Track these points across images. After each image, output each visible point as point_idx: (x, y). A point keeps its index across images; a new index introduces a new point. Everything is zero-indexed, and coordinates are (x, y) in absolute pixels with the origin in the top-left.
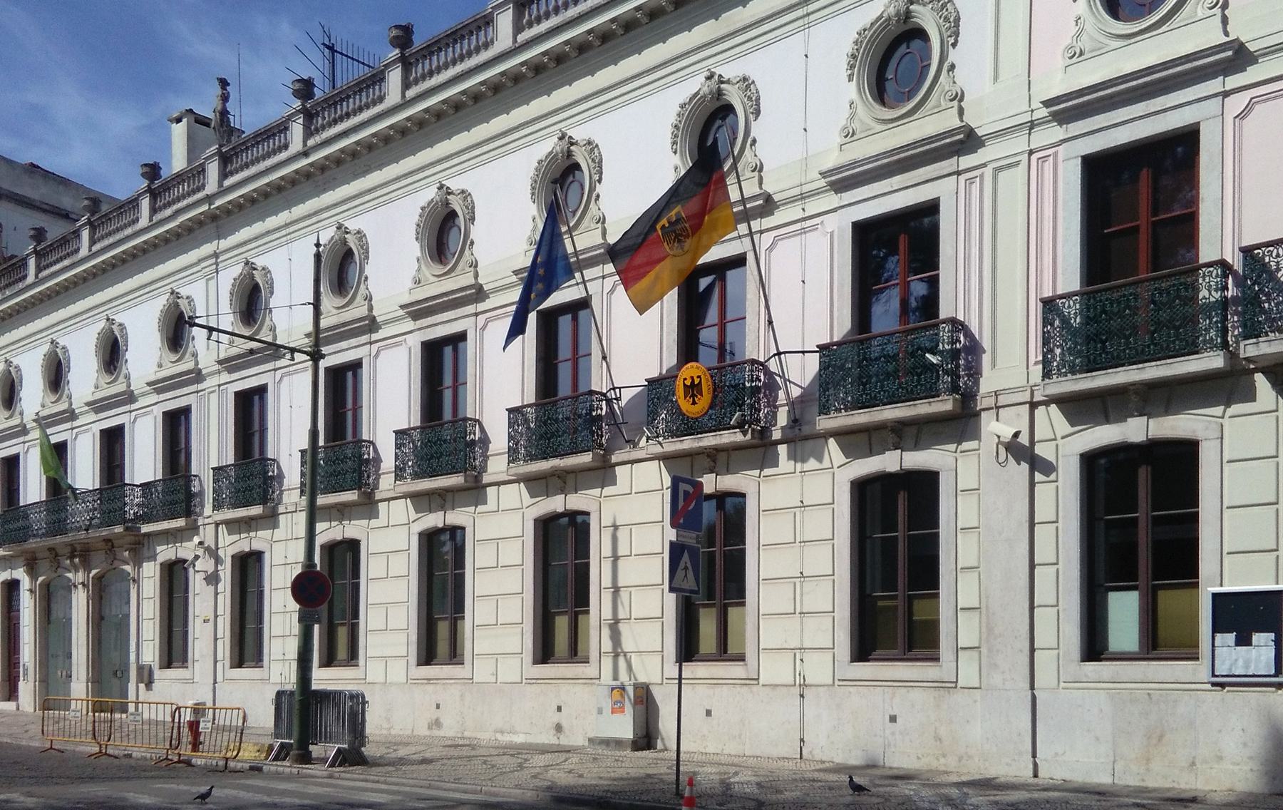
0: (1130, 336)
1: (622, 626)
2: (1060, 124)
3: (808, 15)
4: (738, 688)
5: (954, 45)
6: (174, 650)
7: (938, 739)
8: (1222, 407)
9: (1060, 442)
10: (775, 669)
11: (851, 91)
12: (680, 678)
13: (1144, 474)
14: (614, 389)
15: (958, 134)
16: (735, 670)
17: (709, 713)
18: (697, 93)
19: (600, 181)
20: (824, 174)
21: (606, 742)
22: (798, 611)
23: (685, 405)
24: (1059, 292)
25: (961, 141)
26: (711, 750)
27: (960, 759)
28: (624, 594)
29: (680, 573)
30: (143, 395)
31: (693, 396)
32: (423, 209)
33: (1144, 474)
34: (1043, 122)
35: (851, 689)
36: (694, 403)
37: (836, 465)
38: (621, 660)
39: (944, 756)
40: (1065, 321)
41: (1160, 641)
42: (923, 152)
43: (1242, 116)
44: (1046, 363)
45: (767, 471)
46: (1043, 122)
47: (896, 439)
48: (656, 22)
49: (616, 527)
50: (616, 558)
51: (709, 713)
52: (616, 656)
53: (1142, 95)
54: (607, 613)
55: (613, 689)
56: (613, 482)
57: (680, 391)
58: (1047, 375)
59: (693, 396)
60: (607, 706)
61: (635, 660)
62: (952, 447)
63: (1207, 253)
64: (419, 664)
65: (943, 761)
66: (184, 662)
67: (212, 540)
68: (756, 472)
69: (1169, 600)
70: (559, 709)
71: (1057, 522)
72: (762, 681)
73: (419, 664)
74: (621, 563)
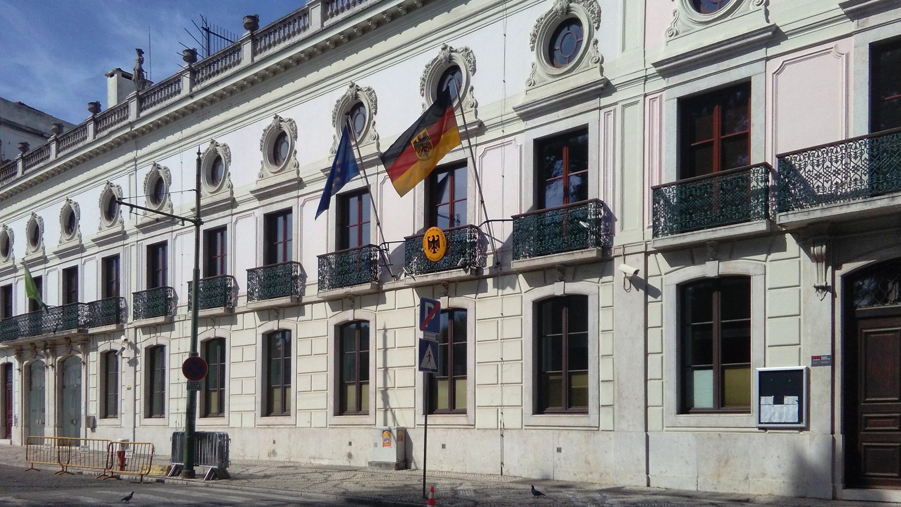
1: (389, 392)
2: (664, 78)
5: (597, 28)
6: (109, 408)
7: (587, 462)
10: (485, 419)
11: (533, 57)
12: (426, 425)
16: (460, 419)
17: (444, 446)
21: (380, 465)
23: (429, 254)
24: (663, 183)
25: (602, 89)
26: (445, 469)
27: (601, 475)
29: (426, 359)
30: (90, 247)
31: (434, 248)
32: (265, 131)
34: (653, 76)
36: (435, 252)
39: (591, 473)
40: (667, 201)
41: (726, 401)
42: (563, 101)
43: (778, 72)
44: (655, 227)
45: (480, 295)
46: (653, 76)
51: (444, 446)
52: (386, 411)
56: (384, 301)
57: (426, 245)
58: (655, 235)
59: (434, 248)
60: (380, 442)
63: (756, 158)
65: (590, 476)
66: (115, 414)
67: (133, 338)
68: (473, 296)
69: (732, 375)
70: (350, 444)
73: (335, 414)
74: (389, 352)
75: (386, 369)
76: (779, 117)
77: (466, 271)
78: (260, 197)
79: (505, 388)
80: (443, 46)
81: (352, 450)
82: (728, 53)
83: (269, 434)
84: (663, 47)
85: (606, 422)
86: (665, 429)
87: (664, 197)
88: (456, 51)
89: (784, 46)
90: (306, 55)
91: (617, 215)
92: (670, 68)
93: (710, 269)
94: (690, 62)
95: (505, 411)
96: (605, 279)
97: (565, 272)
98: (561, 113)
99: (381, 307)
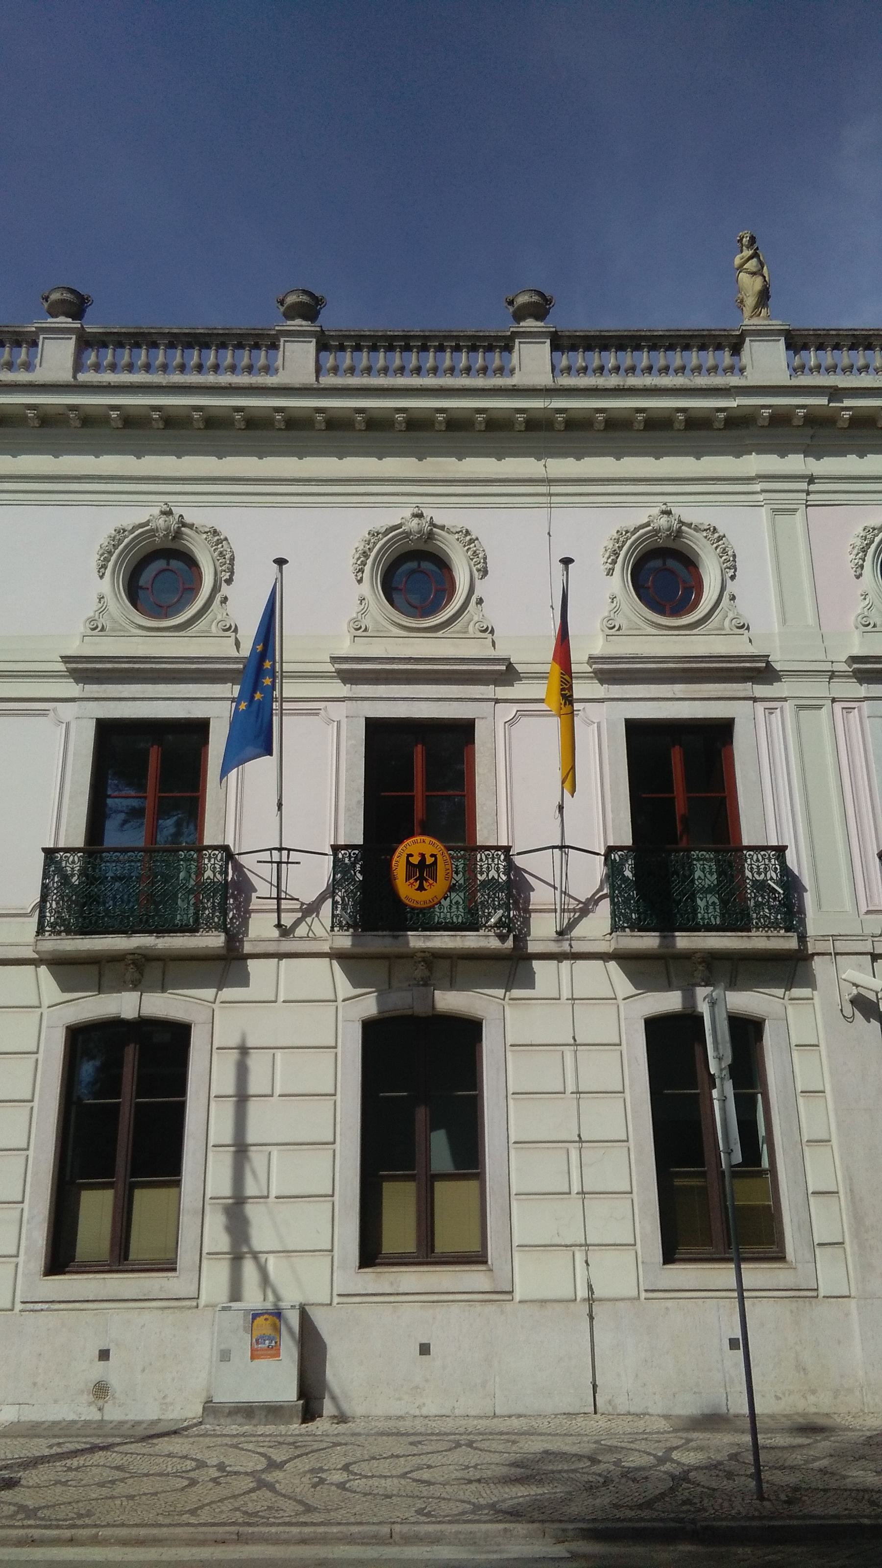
0: (160, 903)
1: (252, 1210)
2: (77, 681)
3: (550, 495)
4: (479, 1307)
5: (733, 578)
7: (801, 1368)
8: (215, 990)
9: (44, 1010)
10: (531, 1277)
11: (105, 586)
12: (740, 1289)
13: (131, 1054)
14: (280, 849)
15: (238, 663)
16: (471, 1278)
17: (425, 1349)
18: (399, 526)
19: (229, 581)
20: (334, 660)
21: (247, 1411)
22: (576, 1188)
24: (61, 845)
25: (758, 670)
26: (431, 1409)
27: (836, 1393)
28: (257, 1157)
31: (421, 879)
32: (374, 534)
33: (131, 1054)
34: (842, 675)
35: (669, 1303)
36: (421, 888)
37: (340, 998)
38: (249, 1269)
39: (814, 1392)
40: (65, 879)
42: (406, 671)
43: (511, 722)
45: (516, 993)
46: (842, 675)
47: (137, 975)
48: (251, 433)
49: (244, 1050)
50: (242, 1098)
51: (425, 1349)
52: (237, 1259)
53: (174, 678)
54: (220, 1182)
55: (255, 1316)
56: (243, 980)
59: (421, 879)
60: (242, 1344)
61: (272, 1264)
62: (780, 992)
64: (780, 1257)
65: (812, 1399)
68: (500, 992)
69: (146, 1201)
70: (104, 1355)
71: (335, 1095)
72: (518, 1296)
73: (780, 1257)
74: (253, 1107)
75: (241, 1149)
76: (246, 790)
77: (503, 938)
78: (348, 677)
79: (592, 1204)
80: (165, 508)
81: (113, 1373)
82: (96, 675)
83: (86, 1332)
84: (78, 642)
85: (830, 1275)
86: (336, 1300)
87: (60, 871)
88: (191, 526)
89: (518, 690)
90: (38, 417)
91: (806, 881)
92: (87, 671)
93: (125, 1005)
94: (98, 670)
95: (595, 1256)
96: (796, 992)
97: (139, 971)
98: (679, 689)
99: (229, 993)
